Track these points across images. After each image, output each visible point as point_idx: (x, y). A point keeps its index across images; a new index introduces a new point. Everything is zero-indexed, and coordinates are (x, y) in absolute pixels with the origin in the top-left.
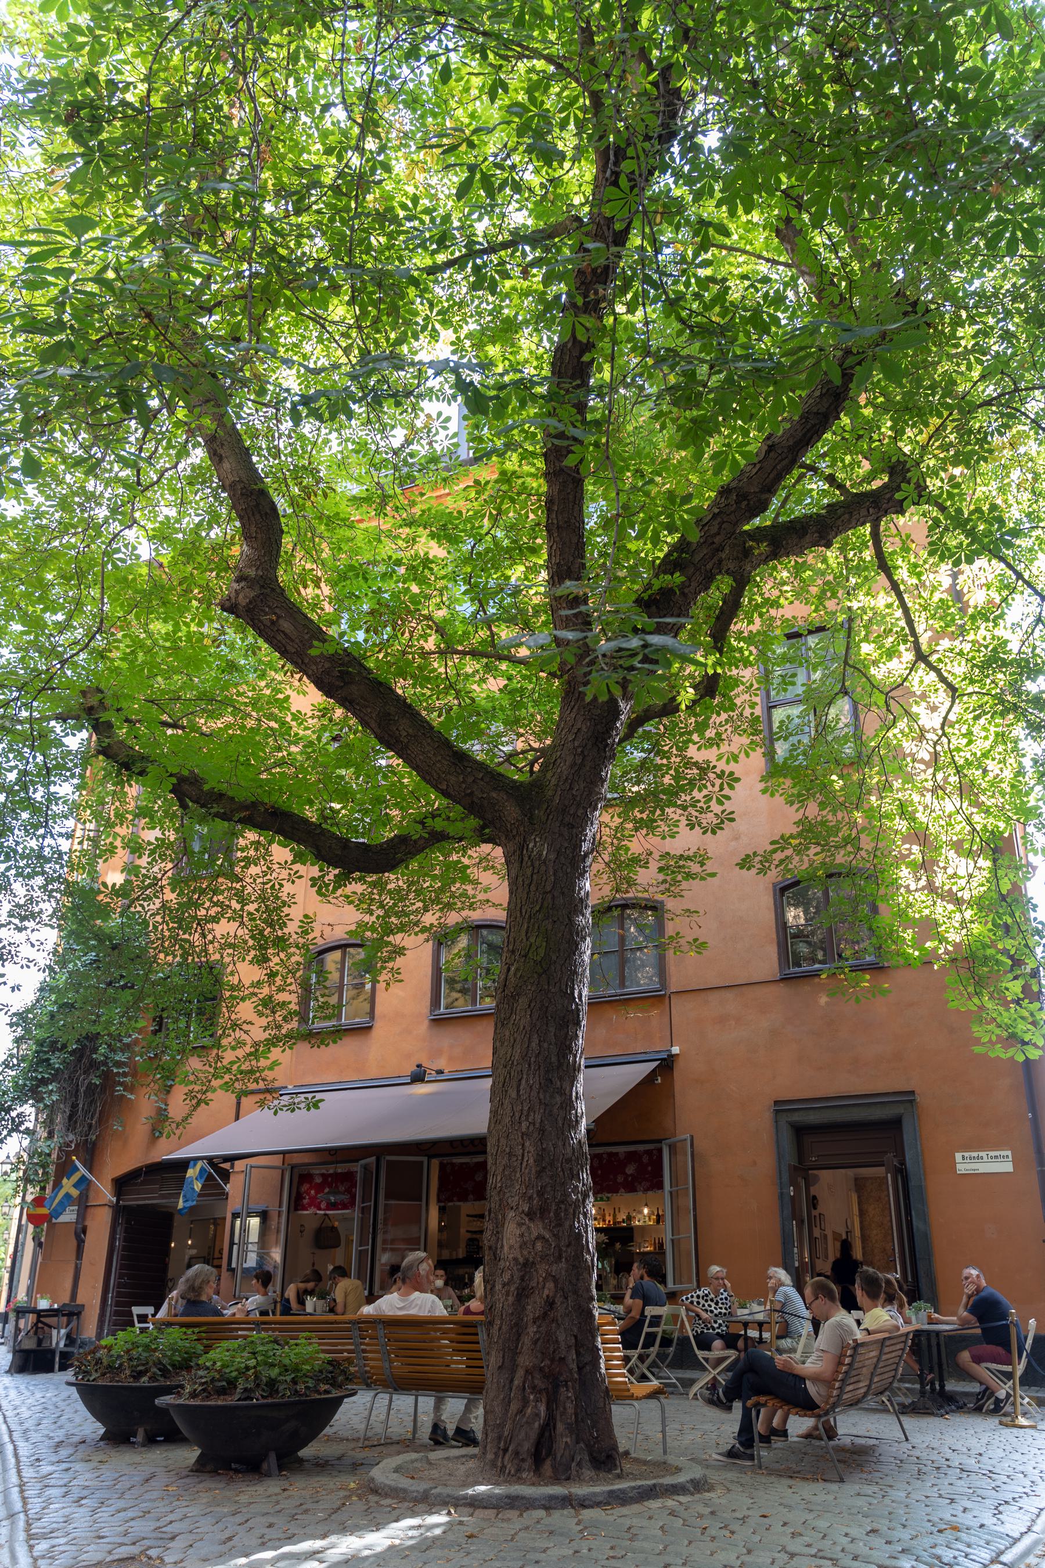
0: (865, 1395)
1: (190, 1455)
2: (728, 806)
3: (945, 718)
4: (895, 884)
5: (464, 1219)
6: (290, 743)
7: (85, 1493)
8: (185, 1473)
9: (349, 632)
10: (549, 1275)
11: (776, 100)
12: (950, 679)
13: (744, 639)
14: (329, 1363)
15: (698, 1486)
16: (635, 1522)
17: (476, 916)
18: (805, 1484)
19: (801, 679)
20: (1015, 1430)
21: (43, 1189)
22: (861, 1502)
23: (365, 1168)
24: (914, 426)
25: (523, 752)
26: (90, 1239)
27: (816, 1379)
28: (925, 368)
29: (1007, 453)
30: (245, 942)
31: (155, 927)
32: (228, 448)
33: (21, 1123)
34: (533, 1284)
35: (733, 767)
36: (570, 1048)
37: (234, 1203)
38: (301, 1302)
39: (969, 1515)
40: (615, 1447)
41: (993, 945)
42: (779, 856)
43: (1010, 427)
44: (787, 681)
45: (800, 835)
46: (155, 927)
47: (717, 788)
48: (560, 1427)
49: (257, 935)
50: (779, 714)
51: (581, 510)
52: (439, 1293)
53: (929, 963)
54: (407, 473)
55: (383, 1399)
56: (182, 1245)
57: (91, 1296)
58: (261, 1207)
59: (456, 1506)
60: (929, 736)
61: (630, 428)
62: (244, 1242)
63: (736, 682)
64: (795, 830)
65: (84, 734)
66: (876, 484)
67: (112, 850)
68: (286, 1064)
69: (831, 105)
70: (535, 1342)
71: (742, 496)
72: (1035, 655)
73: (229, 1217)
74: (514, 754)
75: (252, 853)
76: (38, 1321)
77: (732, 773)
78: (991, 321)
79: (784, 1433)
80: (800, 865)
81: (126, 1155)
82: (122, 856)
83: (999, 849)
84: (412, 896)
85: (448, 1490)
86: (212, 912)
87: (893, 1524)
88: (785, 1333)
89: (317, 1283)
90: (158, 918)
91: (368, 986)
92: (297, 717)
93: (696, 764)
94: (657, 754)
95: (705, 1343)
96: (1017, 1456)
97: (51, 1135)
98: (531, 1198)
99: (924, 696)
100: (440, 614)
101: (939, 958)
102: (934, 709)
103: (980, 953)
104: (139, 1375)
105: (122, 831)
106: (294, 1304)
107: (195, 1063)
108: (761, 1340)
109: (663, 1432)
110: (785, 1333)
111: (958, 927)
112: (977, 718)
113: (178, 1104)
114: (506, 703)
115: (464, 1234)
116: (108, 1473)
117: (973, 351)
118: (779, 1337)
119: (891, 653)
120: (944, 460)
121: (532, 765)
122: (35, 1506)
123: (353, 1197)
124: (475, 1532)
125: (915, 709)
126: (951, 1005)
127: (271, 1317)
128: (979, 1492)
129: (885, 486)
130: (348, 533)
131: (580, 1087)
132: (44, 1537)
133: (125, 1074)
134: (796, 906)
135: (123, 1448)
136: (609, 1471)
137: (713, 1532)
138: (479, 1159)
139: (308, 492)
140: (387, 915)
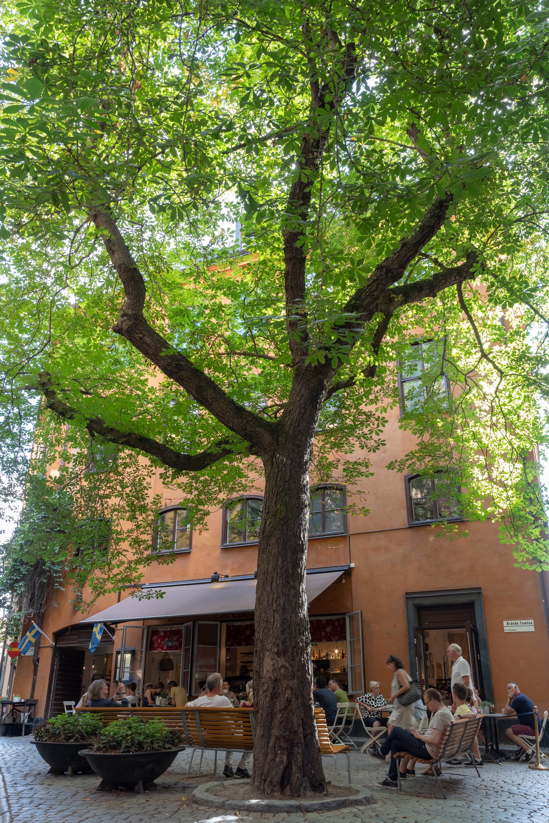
0: (457, 751)
1: (97, 781)
2: (382, 436)
3: (497, 388)
4: (471, 477)
7: (41, 802)
8: (94, 791)
9: (179, 343)
11: (407, 61)
12: (500, 367)
13: (389, 346)
14: (171, 732)
15: (368, 801)
17: (246, 494)
18: (424, 800)
19: (419, 368)
20: (537, 771)
21: (16, 638)
22: (456, 810)
23: (187, 627)
25: (271, 406)
26: (41, 665)
27: (430, 744)
28: (486, 202)
29: (529, 246)
30: (123, 507)
31: (77, 500)
32: (117, 247)
33: (5, 603)
34: (280, 691)
35: (384, 415)
36: (299, 565)
37: (117, 646)
38: (154, 699)
39: (515, 818)
40: (323, 779)
41: (524, 509)
42: (410, 462)
43: (531, 234)
44: (413, 368)
46: (77, 500)
47: (376, 426)
48: (294, 768)
49: (131, 505)
50: (407, 387)
51: (303, 278)
52: (226, 695)
53: (489, 519)
55: (199, 752)
57: (41, 695)
58: (131, 648)
59: (239, 810)
60: (488, 397)
61: (328, 235)
63: (384, 369)
64: (417, 448)
65: (38, 398)
66: (460, 264)
67: (53, 459)
70: (281, 723)
71: (389, 270)
72: (545, 355)
73: (115, 653)
74: (266, 408)
76: (14, 708)
77: (383, 418)
79: (413, 772)
80: (419, 467)
81: (60, 621)
82: (59, 461)
83: (526, 458)
84: (213, 484)
86: (107, 492)
89: (162, 689)
90: (78, 495)
92: (152, 390)
93: (364, 413)
94: (344, 407)
95: (369, 723)
96: (539, 786)
97: (20, 610)
98: (278, 645)
99: (486, 376)
100: (227, 334)
101: (495, 517)
102: (491, 383)
103: (517, 514)
105: (59, 449)
106: (149, 700)
107: (97, 573)
111: (505, 501)
112: (514, 388)
113: (88, 593)
114: (262, 380)
116: (53, 791)
120: (497, 251)
121: (276, 413)
122: (15, 808)
123: (181, 643)
126: (502, 542)
127: (137, 708)
128: (520, 805)
129: (464, 265)
130: (181, 292)
131: (304, 586)
133: (60, 577)
135: (60, 777)
136: (321, 792)
138: (248, 623)
139: (158, 270)
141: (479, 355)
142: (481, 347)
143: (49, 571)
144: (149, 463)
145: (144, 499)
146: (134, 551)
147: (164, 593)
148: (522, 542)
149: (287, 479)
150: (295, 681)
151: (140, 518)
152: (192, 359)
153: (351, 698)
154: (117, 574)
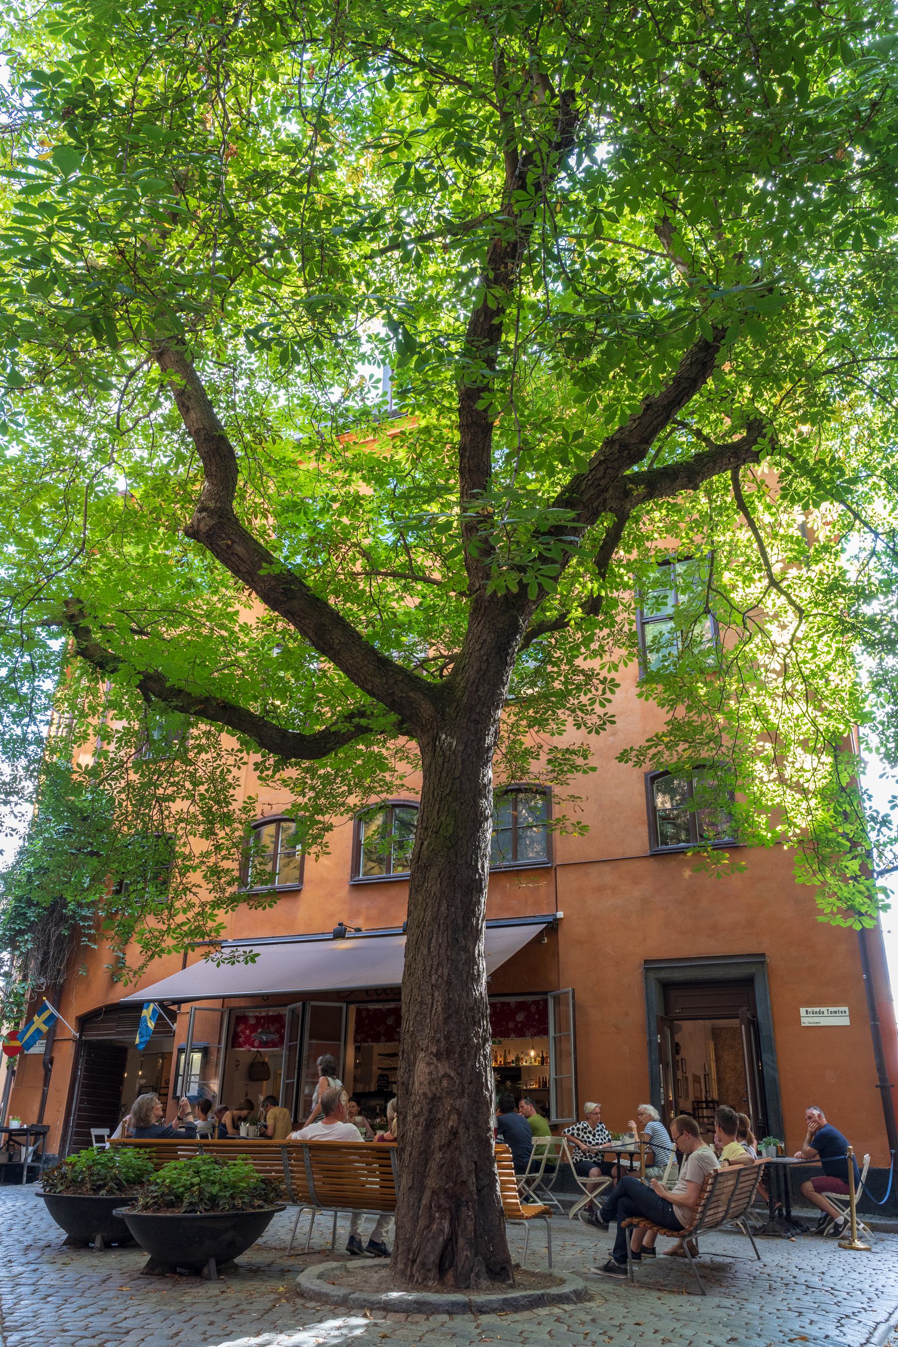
0: (724, 1218)
1: (142, 1259)
2: (610, 709)
3: (794, 635)
4: (750, 777)
5: (376, 1058)
6: (238, 649)
7: (51, 1291)
8: (137, 1275)
9: (289, 555)
10: (453, 1108)
11: (658, 121)
12: (798, 601)
14: (263, 1181)
15: (580, 1296)
16: (526, 1327)
17: (393, 797)
18: (668, 1296)
19: (670, 601)
20: (852, 1252)
21: (17, 1024)
22: (721, 1313)
23: (293, 1011)
24: (771, 389)
25: (435, 659)
26: (56, 1069)
27: (681, 1205)
28: (779, 343)
29: (846, 413)
30: (195, 816)
32: (193, 401)
34: (440, 1116)
35: (613, 674)
36: (473, 912)
37: (180, 1040)
38: (236, 1128)
39: (815, 1327)
40: (508, 1260)
42: (653, 751)
43: (849, 393)
44: (660, 602)
45: (670, 733)
46: (120, 804)
47: (600, 692)
48: (461, 1241)
49: (208, 812)
50: (651, 631)
51: (489, 456)
54: (342, 422)
56: (134, 1076)
58: (203, 1044)
59: (371, 1309)
60: (779, 650)
61: (529, 389)
62: (188, 1074)
63: (615, 602)
64: (666, 729)
66: (736, 438)
67: (85, 737)
68: (228, 922)
69: (704, 127)
70: (441, 1167)
71: (624, 446)
72: (870, 584)
74: (426, 660)
75: (204, 741)
77: (613, 680)
78: (833, 304)
79: (653, 1251)
80: (669, 759)
84: (338, 780)
85: (364, 1296)
86: (169, 791)
87: (750, 1333)
88: (653, 1161)
90: (123, 796)
91: (298, 858)
92: (245, 628)
93: (583, 672)
94: (550, 662)
95: (583, 1171)
96: (854, 1275)
97: (25, 978)
98: (438, 1041)
99: (776, 616)
100: (366, 542)
102: (783, 627)
103: (823, 837)
104: (100, 1187)
105: (95, 721)
107: (151, 922)
108: (632, 1169)
109: (549, 1248)
110: (653, 1161)
111: (805, 816)
112: (820, 636)
113: (134, 953)
114: (421, 617)
115: (375, 1071)
116: (70, 1273)
117: (819, 327)
118: (648, 1166)
119: (748, 579)
121: (441, 669)
123: (282, 1037)
124: (388, 1332)
125: (768, 627)
126: (799, 881)
128: (824, 1306)
129: (743, 440)
131: (481, 946)
132: (16, 1329)
133: (90, 927)
134: (664, 793)
135: (83, 1252)
136: (503, 1281)
137: (594, 1337)
138: (392, 1005)
139: (259, 439)
140: (317, 797)
141: (766, 582)
142: (769, 570)
143: (73, 918)
144: (237, 746)
145: (228, 804)
146: (211, 886)
147: (257, 955)
148: (831, 881)
149: (457, 774)
150: (465, 1100)
151: (222, 834)
152: (310, 582)
153: (555, 1129)
154: (183, 924)
